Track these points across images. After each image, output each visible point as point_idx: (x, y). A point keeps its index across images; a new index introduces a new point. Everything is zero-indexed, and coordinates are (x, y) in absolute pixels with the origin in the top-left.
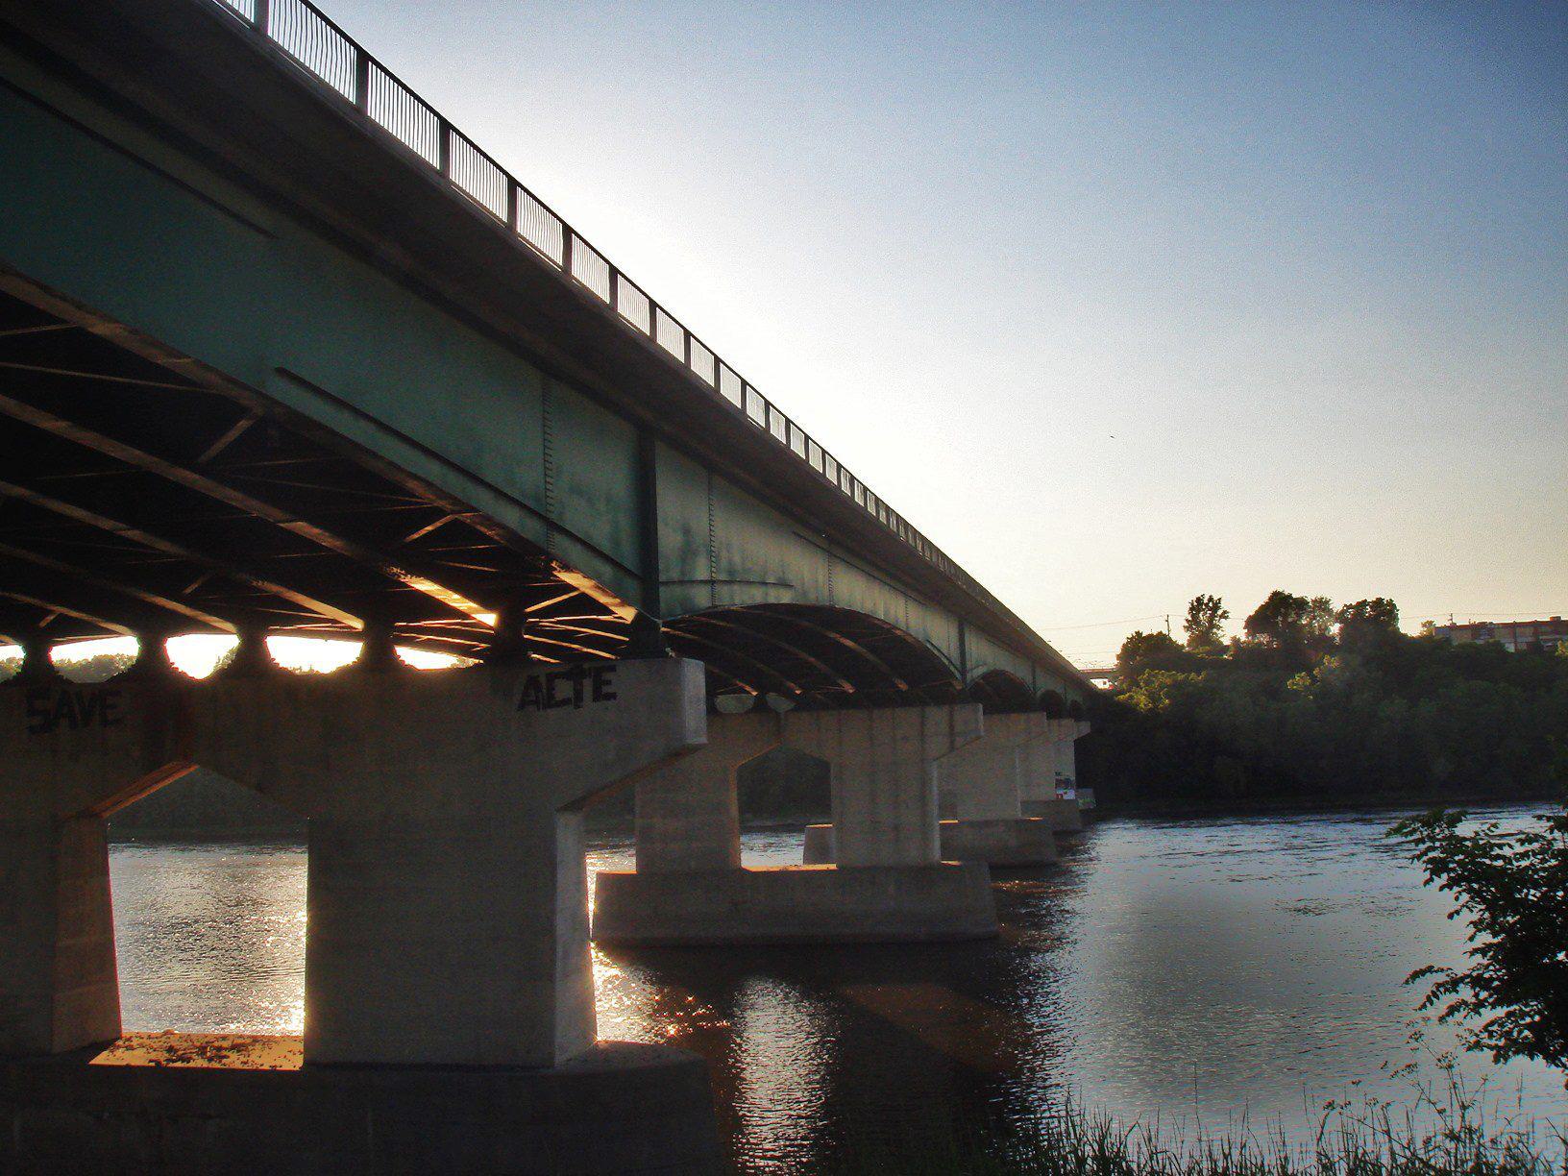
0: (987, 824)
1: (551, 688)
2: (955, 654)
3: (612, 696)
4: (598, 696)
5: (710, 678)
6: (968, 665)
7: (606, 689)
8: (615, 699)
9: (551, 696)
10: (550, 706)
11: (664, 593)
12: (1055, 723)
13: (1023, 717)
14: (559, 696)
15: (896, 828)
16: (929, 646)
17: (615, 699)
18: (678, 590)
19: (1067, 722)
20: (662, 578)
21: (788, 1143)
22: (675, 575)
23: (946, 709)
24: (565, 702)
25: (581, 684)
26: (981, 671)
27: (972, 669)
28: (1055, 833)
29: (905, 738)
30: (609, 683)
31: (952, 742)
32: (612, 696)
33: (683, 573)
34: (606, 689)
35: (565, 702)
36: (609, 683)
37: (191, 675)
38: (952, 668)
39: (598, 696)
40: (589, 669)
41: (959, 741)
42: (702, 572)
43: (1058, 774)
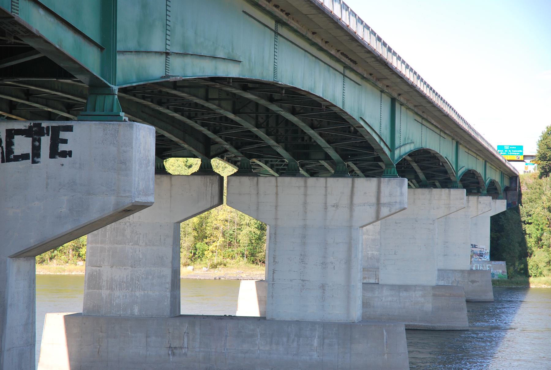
0: (406, 288)
1: (10, 144)
2: (386, 134)
3: (67, 154)
4: (54, 153)
5: (159, 139)
6: (397, 143)
7: (62, 147)
8: (70, 156)
9: (10, 151)
10: (9, 160)
11: (121, 60)
12: (473, 199)
13: (445, 191)
14: (18, 150)
15: (323, 287)
16: (362, 123)
17: (70, 156)
18: (134, 59)
19: (486, 200)
20: (120, 46)
21: (98, 273)
22: (132, 45)
23: (374, 181)
24: (25, 157)
25: (39, 141)
26: (408, 148)
27: (400, 147)
28: (468, 301)
29: (336, 206)
30: (65, 141)
31: (378, 212)
32: (67, 154)
33: (139, 43)
34: (62, 147)
35: (25, 157)
36: (65, 141)
37: (39, 364)
38: (382, 145)
39: (54, 153)
40: (48, 127)
41: (385, 211)
42: (157, 44)
43: (474, 246)
